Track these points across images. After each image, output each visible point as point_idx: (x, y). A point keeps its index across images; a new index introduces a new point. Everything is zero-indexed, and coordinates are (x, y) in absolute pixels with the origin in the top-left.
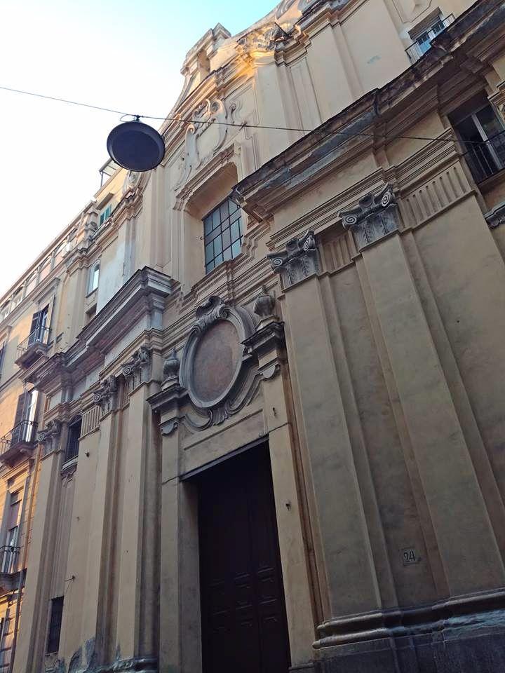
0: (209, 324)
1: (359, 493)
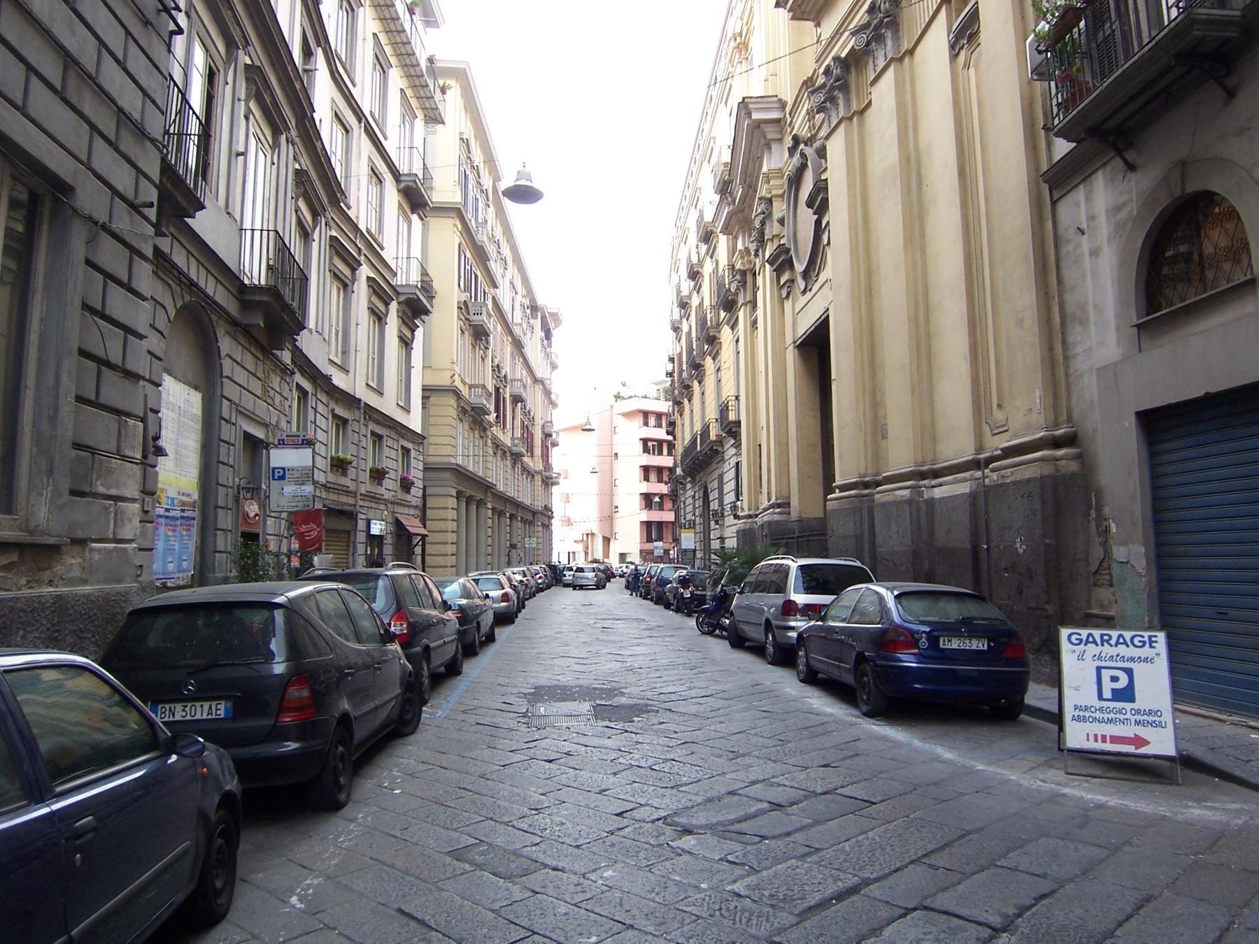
1: (956, 476)
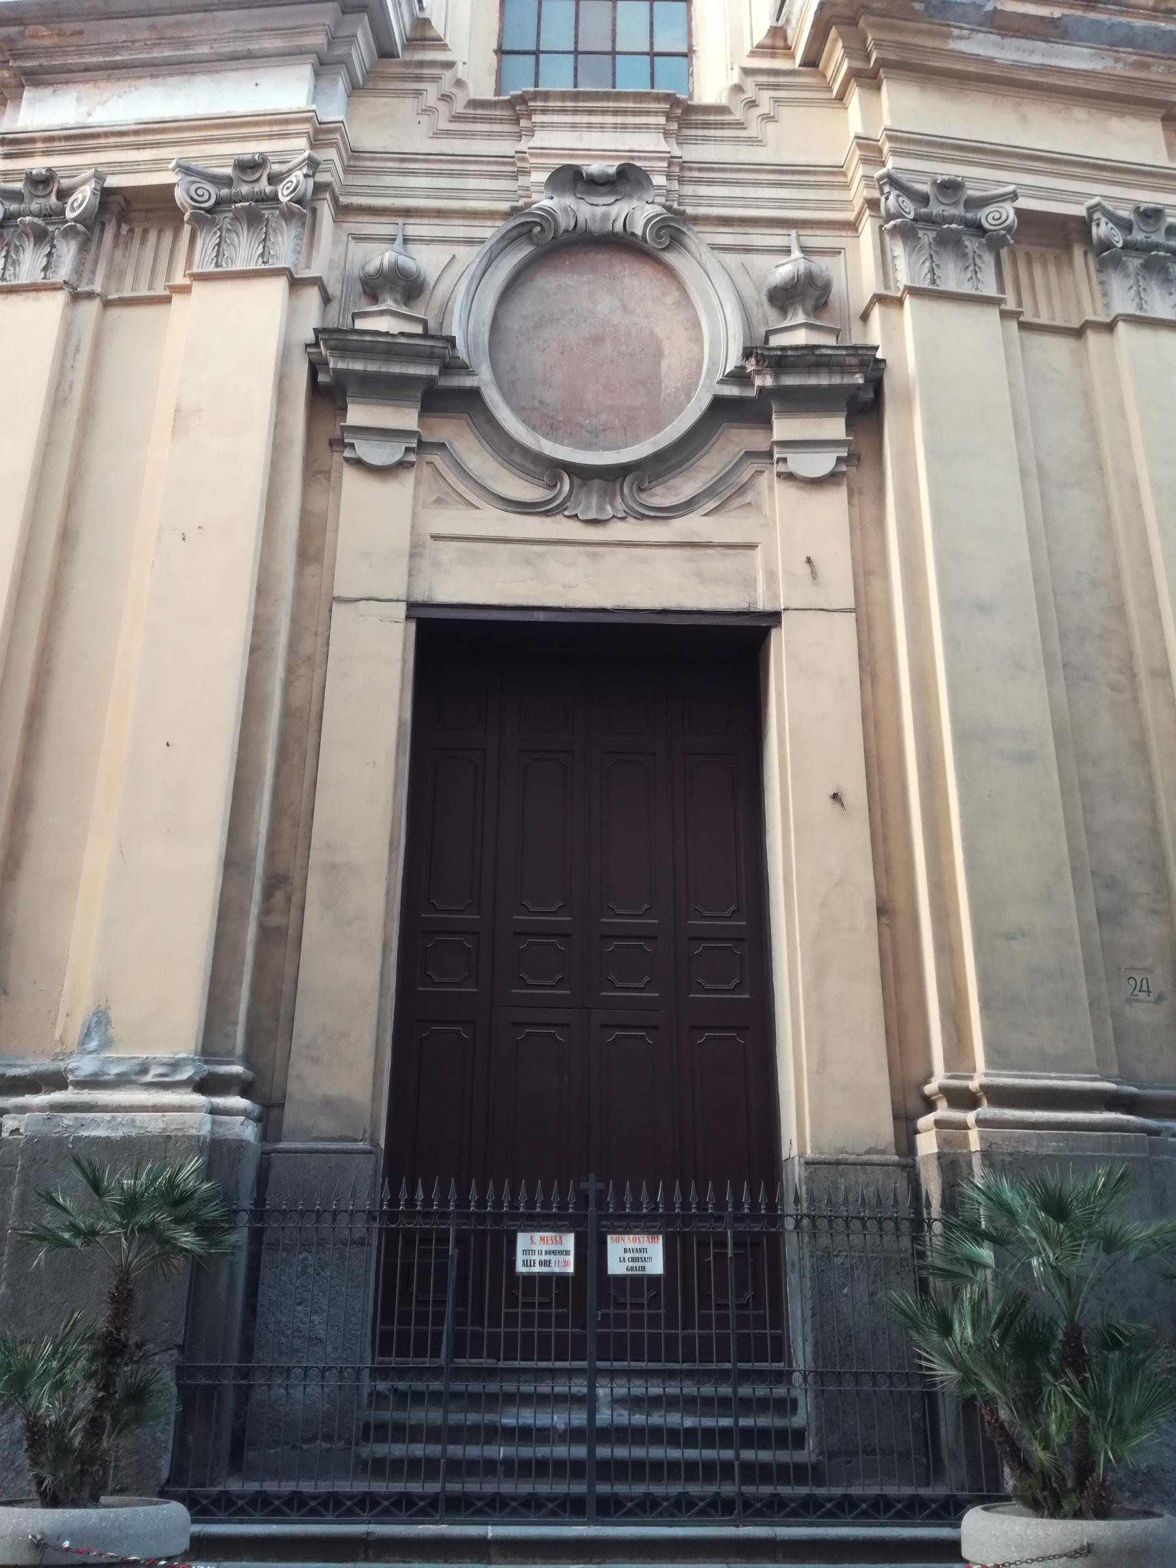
0: (586, 231)
